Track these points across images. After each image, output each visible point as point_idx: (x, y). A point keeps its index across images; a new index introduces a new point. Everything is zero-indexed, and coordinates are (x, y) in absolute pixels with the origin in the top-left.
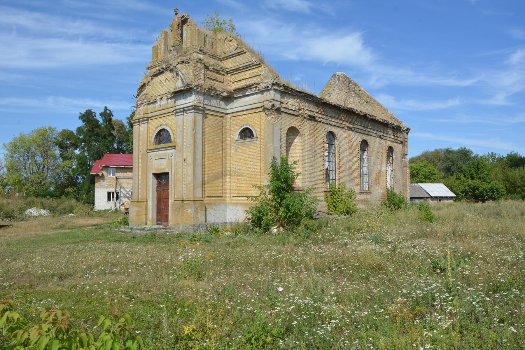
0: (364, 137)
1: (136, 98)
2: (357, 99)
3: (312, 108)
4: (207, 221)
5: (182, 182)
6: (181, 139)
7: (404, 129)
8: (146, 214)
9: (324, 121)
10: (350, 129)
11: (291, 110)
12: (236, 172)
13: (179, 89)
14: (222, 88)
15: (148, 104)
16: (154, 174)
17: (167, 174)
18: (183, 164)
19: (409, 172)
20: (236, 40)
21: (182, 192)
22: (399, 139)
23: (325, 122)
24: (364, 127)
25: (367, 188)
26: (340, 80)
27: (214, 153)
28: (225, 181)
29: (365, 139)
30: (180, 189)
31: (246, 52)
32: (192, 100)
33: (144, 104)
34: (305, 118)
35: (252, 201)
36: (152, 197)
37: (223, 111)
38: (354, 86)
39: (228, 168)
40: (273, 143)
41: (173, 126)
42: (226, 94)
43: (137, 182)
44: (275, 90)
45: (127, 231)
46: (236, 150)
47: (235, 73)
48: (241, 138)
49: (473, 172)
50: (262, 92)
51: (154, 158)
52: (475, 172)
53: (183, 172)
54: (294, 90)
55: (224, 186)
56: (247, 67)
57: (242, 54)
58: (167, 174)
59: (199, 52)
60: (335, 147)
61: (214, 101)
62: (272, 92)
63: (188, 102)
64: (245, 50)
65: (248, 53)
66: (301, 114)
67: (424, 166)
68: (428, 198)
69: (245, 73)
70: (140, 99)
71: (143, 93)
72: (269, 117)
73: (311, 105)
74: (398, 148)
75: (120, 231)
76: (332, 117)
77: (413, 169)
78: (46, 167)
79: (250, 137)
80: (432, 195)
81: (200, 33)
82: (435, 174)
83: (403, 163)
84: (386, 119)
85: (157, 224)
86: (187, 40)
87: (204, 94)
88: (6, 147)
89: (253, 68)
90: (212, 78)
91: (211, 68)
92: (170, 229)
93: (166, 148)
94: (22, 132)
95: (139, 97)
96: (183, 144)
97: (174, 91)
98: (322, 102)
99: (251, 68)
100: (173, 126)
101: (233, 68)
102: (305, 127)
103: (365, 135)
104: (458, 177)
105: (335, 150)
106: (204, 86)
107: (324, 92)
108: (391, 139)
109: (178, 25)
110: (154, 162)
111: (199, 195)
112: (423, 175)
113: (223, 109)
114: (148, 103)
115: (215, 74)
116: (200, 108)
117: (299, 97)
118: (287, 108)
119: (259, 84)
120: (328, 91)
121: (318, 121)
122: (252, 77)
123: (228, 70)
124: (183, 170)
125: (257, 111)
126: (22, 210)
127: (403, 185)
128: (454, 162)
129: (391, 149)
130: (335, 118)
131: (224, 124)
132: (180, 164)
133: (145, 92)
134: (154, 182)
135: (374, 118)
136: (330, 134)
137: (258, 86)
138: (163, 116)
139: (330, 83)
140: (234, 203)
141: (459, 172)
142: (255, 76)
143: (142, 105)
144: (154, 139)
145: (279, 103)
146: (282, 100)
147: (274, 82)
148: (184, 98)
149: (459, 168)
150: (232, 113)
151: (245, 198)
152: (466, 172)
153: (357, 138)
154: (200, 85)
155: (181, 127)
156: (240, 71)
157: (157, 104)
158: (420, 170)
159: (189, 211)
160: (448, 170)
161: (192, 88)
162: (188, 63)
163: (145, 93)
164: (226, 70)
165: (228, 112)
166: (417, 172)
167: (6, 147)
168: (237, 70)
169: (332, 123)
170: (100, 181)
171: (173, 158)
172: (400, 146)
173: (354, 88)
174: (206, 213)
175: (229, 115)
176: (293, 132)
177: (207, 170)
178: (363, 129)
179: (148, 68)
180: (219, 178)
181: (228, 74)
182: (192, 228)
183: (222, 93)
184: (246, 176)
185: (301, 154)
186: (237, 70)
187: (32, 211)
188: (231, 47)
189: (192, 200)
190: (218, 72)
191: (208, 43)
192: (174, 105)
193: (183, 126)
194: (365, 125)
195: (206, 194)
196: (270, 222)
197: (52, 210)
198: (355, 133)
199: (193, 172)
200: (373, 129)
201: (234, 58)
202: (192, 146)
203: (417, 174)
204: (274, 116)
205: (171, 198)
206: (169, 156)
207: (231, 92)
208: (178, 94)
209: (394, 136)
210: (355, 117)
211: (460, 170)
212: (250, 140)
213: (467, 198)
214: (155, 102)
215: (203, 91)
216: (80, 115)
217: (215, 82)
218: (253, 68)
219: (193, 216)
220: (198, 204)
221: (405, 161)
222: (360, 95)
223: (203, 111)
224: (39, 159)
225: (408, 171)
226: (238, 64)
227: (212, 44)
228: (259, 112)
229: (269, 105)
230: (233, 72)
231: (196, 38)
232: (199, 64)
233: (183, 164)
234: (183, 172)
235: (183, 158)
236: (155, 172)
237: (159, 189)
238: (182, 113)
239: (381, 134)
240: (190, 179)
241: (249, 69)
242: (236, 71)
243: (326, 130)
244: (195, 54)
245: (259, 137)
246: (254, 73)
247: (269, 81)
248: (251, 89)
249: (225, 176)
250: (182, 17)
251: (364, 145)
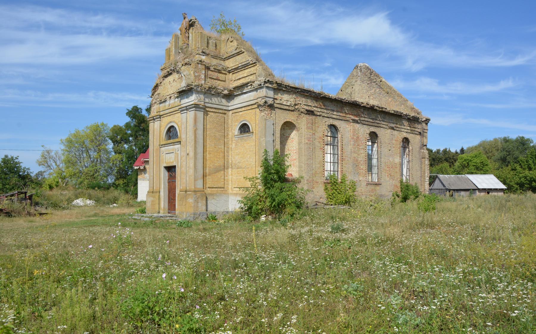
0: (373, 129)
1: (151, 97)
2: (378, 90)
3: (310, 102)
4: (209, 210)
5: (186, 174)
6: (185, 135)
7: (423, 120)
8: (159, 204)
9: (323, 114)
10: (355, 121)
11: (286, 105)
12: (236, 164)
13: (181, 90)
14: (223, 87)
15: (160, 103)
16: (166, 167)
17: (174, 167)
18: (186, 158)
19: (429, 163)
20: (237, 40)
21: (186, 184)
22: (416, 130)
23: (326, 116)
24: (373, 119)
25: (377, 179)
26: (363, 71)
27: (215, 147)
28: (227, 173)
29: (373, 131)
30: (185, 180)
31: (244, 52)
32: (193, 99)
33: (157, 103)
34: (302, 112)
35: (244, 192)
36: (164, 188)
37: (225, 108)
38: (376, 77)
39: (230, 161)
40: (265, 137)
41: (179, 123)
42: (227, 92)
43: (152, 175)
44: (267, 87)
45: (138, 218)
46: (236, 145)
47: (235, 72)
48: (241, 133)
49: (531, 162)
50: (256, 90)
51: (165, 153)
52: (533, 162)
53: (186, 166)
54: (288, 86)
55: (226, 178)
56: (245, 66)
57: (241, 53)
58: (174, 167)
59: (201, 54)
60: (338, 140)
61: (216, 99)
62: (264, 90)
63: (190, 101)
64: (243, 50)
65: (245, 53)
66: (297, 109)
67: (476, 156)
68: (476, 189)
69: (243, 72)
70: (154, 98)
71: (156, 93)
72: (262, 113)
73: (308, 100)
74: (415, 140)
75: (133, 219)
76: (333, 111)
77: (463, 160)
78: (99, 160)
79: (248, 132)
80: (480, 187)
81: (203, 36)
82: (487, 165)
83: (421, 154)
84: (398, 110)
85: (169, 213)
86: (192, 43)
87: (205, 93)
88: (63, 143)
89: (250, 66)
90: (213, 77)
91: (212, 68)
92: (176, 217)
93: (174, 144)
94: (77, 129)
95: (154, 97)
96: (187, 140)
97: (178, 91)
98: (321, 96)
99: (248, 67)
100: (179, 123)
101: (234, 68)
102: (303, 122)
103: (375, 127)
104: (514, 168)
105: (338, 143)
106: (204, 86)
107: (347, 83)
108: (405, 131)
109: (186, 29)
110: (165, 156)
111: (200, 185)
112: (474, 166)
113: (225, 106)
114: (160, 102)
115: (216, 74)
116: (201, 106)
117: (295, 93)
118: (281, 104)
119: (253, 82)
120: (351, 82)
121: (317, 115)
122: (249, 76)
123: (230, 69)
124: (186, 163)
125: (253, 108)
126: (70, 201)
127: (421, 177)
128: (510, 152)
129: (406, 141)
130: (337, 111)
131: (226, 121)
132: (184, 158)
133: (158, 92)
134: (165, 174)
135: (384, 110)
136: (332, 126)
137: (253, 84)
138: (171, 114)
139: (353, 74)
140: (234, 194)
141: (516, 162)
142: (252, 75)
143: (156, 104)
144: (165, 135)
145: (272, 99)
146: (276, 97)
147: (266, 80)
148: (187, 98)
149: (515, 159)
151: (238, 189)
152: (523, 162)
153: (364, 131)
154: (200, 85)
155: (185, 124)
156: (239, 70)
157: (167, 103)
158: (471, 161)
159: (191, 200)
160: (504, 161)
161: (192, 88)
162: (190, 65)
163: (158, 92)
164: (228, 69)
165: (230, 108)
166: (468, 163)
167: (63, 143)
168: (236, 70)
169: (334, 116)
170: (141, 174)
171: (179, 152)
172: (418, 137)
173: (376, 79)
174: (207, 203)
175: (230, 112)
176: (288, 126)
177: (208, 163)
178: (371, 121)
179: (161, 70)
180: (221, 170)
181: (230, 73)
182: (192, 216)
183: (223, 91)
184: (244, 168)
185: (297, 147)
186: (236, 70)
187: (79, 202)
188: (231, 48)
189: (193, 190)
190: (219, 72)
191: (211, 44)
192: (180, 104)
193: (187, 123)
194: (374, 117)
195: (208, 185)
196: (260, 211)
197: (97, 200)
198: (362, 125)
199: (194, 165)
200: (383, 121)
201: (235, 58)
202: (193, 141)
203: (468, 165)
204: (267, 111)
205: (178, 188)
206: (176, 151)
207: (230, 90)
208: (183, 93)
209: (410, 127)
210: (362, 110)
211: (516, 160)
212: (247, 134)
213: (523, 190)
214: (165, 101)
215: (204, 91)
216: (127, 111)
217: (216, 81)
218: (250, 66)
219: (194, 206)
220: (198, 194)
221: (423, 152)
222: (381, 86)
223: (204, 109)
224: (93, 154)
225: (426, 162)
226: (237, 63)
227: (216, 45)
228: (254, 108)
229: (262, 102)
230: (234, 71)
231: (199, 41)
232: (200, 65)
233: (186, 158)
234: (186, 166)
235: (186, 152)
236: (166, 165)
237: (170, 181)
238: (186, 111)
239: (393, 125)
240: (191, 171)
241: (247, 68)
242: (236, 70)
243: (327, 123)
244: (197, 56)
245: (255, 132)
246: (250, 72)
247: (262, 79)
248: (247, 86)
249: (227, 169)
250: (190, 21)
251: (373, 137)
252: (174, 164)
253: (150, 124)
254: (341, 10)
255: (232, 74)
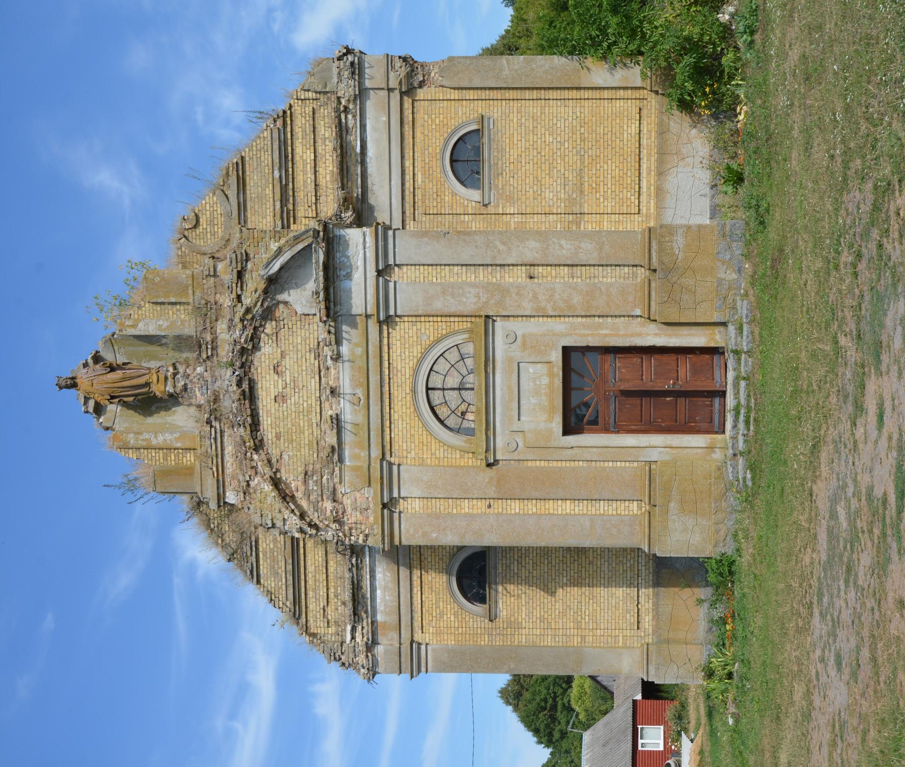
47: (291, 207)
99: (289, 142)
123: (279, 223)
148: (349, 276)
150: (403, 213)
157: (349, 416)
212: (485, 140)
228: (413, 113)
246: (304, 131)
252: (557, 357)
253: (403, 544)
254: (141, 343)
255: (294, 223)
